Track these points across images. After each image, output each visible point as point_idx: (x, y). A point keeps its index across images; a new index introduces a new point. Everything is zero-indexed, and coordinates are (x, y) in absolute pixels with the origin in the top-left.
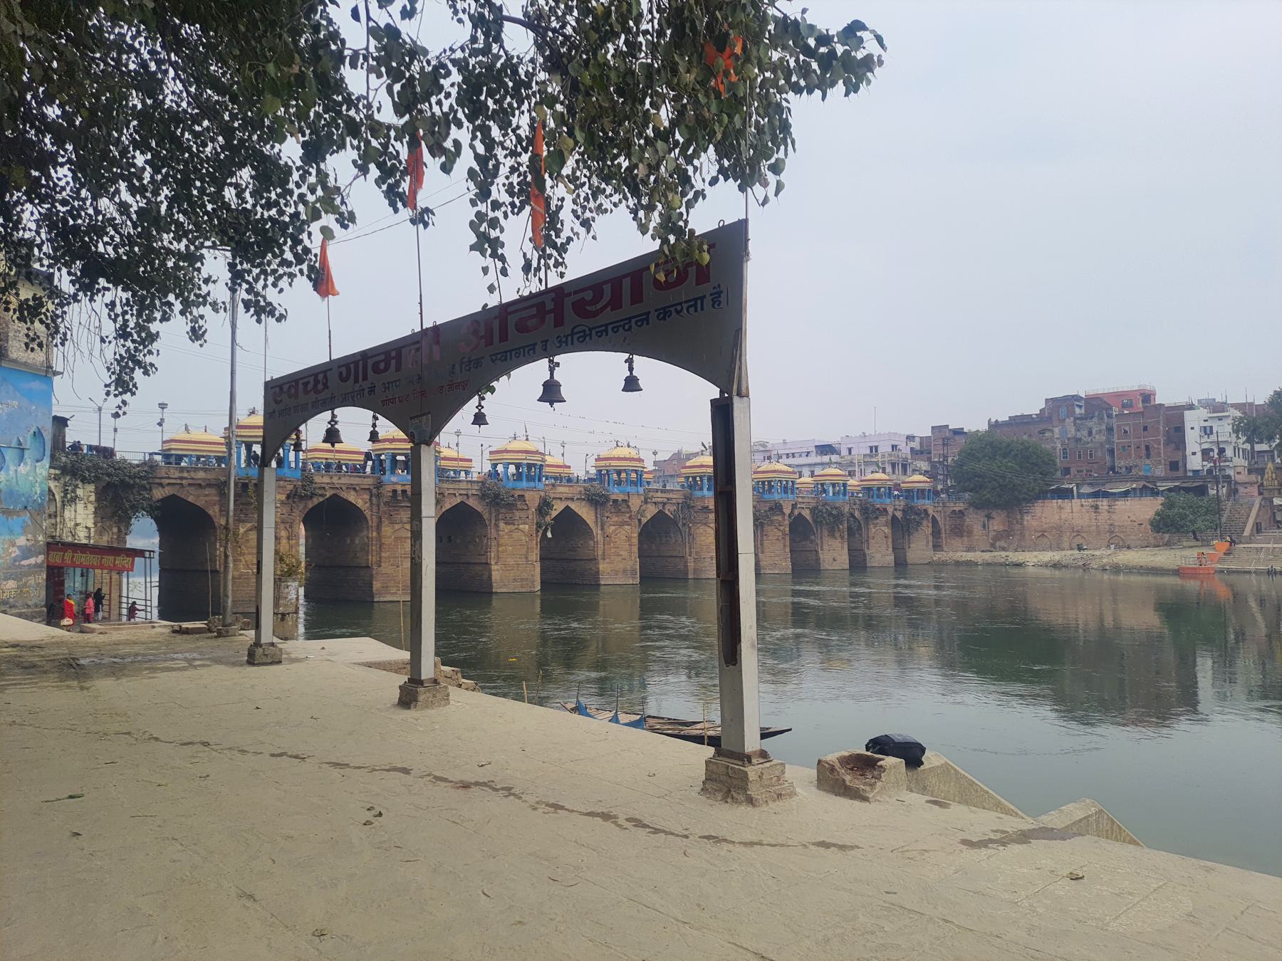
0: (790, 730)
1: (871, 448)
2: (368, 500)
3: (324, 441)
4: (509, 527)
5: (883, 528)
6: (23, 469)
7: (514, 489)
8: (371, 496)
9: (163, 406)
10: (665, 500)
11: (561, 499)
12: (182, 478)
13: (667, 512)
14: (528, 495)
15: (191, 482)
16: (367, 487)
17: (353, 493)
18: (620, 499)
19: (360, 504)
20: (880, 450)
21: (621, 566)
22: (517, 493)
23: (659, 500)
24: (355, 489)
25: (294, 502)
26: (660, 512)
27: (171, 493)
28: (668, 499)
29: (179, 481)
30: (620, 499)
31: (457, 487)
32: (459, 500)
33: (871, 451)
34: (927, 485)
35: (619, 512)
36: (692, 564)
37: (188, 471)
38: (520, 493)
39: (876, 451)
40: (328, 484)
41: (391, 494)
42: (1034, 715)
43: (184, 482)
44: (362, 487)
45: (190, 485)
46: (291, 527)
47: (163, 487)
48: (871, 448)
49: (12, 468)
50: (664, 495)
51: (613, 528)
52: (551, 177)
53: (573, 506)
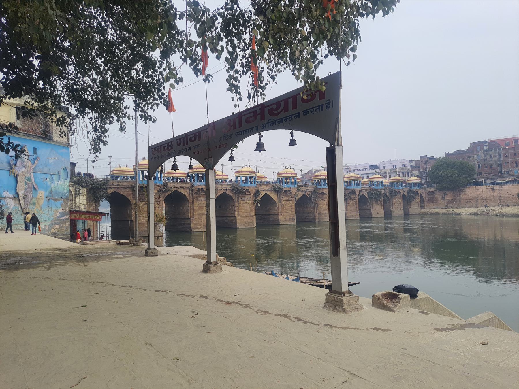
0: (360, 283)
1: (393, 166)
4: (243, 202)
5: (399, 200)
6: (60, 183)
7: (244, 187)
8: (190, 191)
9: (110, 157)
10: (306, 190)
12: (118, 185)
13: (307, 195)
14: (250, 189)
15: (122, 186)
16: (188, 187)
17: (182, 189)
18: (287, 190)
19: (185, 193)
21: (288, 217)
22: (246, 188)
23: (304, 190)
24: (183, 188)
29: (117, 186)
31: (222, 186)
33: (394, 167)
34: (418, 181)
35: (287, 195)
36: (317, 216)
37: (120, 182)
39: (396, 167)
43: (119, 186)
45: (121, 187)
46: (159, 203)
47: (111, 189)
48: (393, 166)
49: (56, 182)
50: (305, 188)
51: (284, 201)
53: (268, 193)
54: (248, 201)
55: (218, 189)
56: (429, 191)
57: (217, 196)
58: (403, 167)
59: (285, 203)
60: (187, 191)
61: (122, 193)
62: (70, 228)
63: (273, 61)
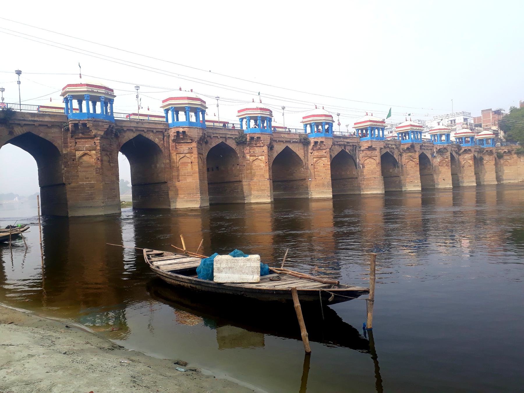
1: (451, 121)
2: (162, 139)
3: (300, 338)
4: (252, 158)
5: (469, 161)
8: (164, 137)
9: (19, 73)
10: (346, 143)
11: (283, 141)
12: (34, 121)
13: (347, 151)
17: (151, 134)
18: (319, 141)
19: (157, 141)
20: (457, 122)
23: (342, 143)
24: (153, 131)
25: (112, 139)
26: (342, 150)
27: (28, 131)
28: (348, 143)
29: (32, 123)
30: (319, 141)
32: (220, 141)
33: (452, 123)
34: (491, 136)
38: (258, 136)
39: (455, 123)
40: (134, 127)
41: (176, 134)
42: (488, 259)
43: (35, 123)
44: (157, 130)
45: (40, 125)
46: (110, 154)
47: (22, 127)
48: (451, 121)
52: (246, 139)
53: (291, 146)
54: (260, 157)
55: (212, 137)
56: (504, 150)
57: (275, 155)
58: (464, 121)
59: (316, 161)
60: (160, 136)
61: (41, 135)
62: (199, 173)
63: (337, 144)
